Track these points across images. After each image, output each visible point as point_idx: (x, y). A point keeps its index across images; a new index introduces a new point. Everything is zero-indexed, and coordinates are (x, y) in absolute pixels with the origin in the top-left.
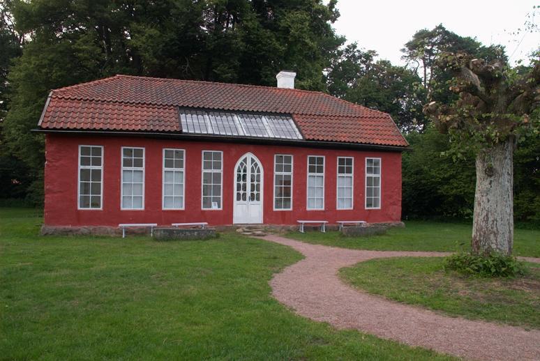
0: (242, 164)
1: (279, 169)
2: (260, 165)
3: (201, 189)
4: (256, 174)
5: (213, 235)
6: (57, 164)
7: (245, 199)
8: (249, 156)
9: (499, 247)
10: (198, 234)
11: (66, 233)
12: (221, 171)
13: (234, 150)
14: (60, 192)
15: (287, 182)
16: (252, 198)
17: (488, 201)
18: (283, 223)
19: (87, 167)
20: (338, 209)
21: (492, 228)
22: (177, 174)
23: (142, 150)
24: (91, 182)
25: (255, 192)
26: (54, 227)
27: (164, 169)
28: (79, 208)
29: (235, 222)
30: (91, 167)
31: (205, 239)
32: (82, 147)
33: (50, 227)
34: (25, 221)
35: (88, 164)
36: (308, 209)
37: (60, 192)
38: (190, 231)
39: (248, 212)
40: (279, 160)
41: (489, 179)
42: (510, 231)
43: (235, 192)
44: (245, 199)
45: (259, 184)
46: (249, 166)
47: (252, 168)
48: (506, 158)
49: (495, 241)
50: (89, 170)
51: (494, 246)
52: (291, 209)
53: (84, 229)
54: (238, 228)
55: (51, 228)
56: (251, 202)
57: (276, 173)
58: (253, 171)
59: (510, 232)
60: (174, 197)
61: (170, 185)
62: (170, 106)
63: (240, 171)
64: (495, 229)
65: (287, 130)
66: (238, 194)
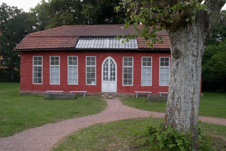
0: (106, 62)
1: (126, 64)
2: (115, 63)
4: (113, 67)
5: (73, 98)
6: (25, 65)
7: (107, 80)
8: (109, 58)
9: (180, 123)
10: (65, 97)
11: (28, 94)
12: (95, 66)
13: (101, 56)
14: (26, 76)
15: (40, 70)
16: (111, 79)
17: (175, 80)
18: (128, 93)
19: (36, 66)
20: (160, 85)
21: (177, 105)
22: (148, 69)
26: (23, 91)
27: (69, 66)
28: (33, 83)
29: (102, 91)
30: (128, 67)
31: (69, 100)
32: (34, 57)
33: (22, 91)
34: (15, 88)
35: (36, 64)
36: (142, 85)
37: (26, 76)
38: (61, 95)
39: (109, 86)
40: (126, 60)
41: (176, 62)
42: (193, 109)
44: (107, 80)
46: (109, 63)
48: (189, 41)
49: (178, 117)
50: (37, 67)
51: (177, 122)
52: (132, 85)
53: (35, 92)
54: (104, 94)
55: (22, 92)
57: (124, 66)
58: (111, 65)
59: (193, 109)
60: (73, 79)
61: (53, 73)
62: (75, 37)
64: (179, 106)
65: (133, 44)
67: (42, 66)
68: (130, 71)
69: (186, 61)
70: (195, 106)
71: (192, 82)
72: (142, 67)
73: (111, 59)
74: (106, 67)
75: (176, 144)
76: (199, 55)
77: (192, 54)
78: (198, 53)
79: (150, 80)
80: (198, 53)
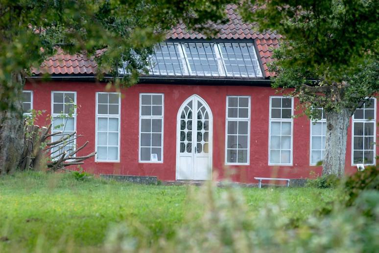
0: (186, 109)
1: (233, 114)
3: (138, 138)
8: (195, 99)
12: (161, 117)
13: (177, 92)
16: (199, 149)
17: (329, 145)
22: (284, 124)
23: (161, 96)
24: (151, 133)
25: (203, 142)
29: (178, 177)
30: (238, 119)
42: (340, 164)
43: (375, 136)
45: (182, 129)
46: (195, 111)
47: (199, 113)
52: (248, 164)
56: (198, 154)
57: (228, 119)
59: (340, 164)
63: (184, 117)
64: (331, 163)
66: (182, 145)
67: (291, 120)
68: (369, 131)
69: (335, 132)
70: (341, 162)
71: (340, 146)
72: (271, 120)
73: (198, 101)
74: (186, 120)
75: (307, 41)
76: (345, 128)
77: (340, 128)
78: (343, 127)
79: (290, 151)
80: (343, 127)
